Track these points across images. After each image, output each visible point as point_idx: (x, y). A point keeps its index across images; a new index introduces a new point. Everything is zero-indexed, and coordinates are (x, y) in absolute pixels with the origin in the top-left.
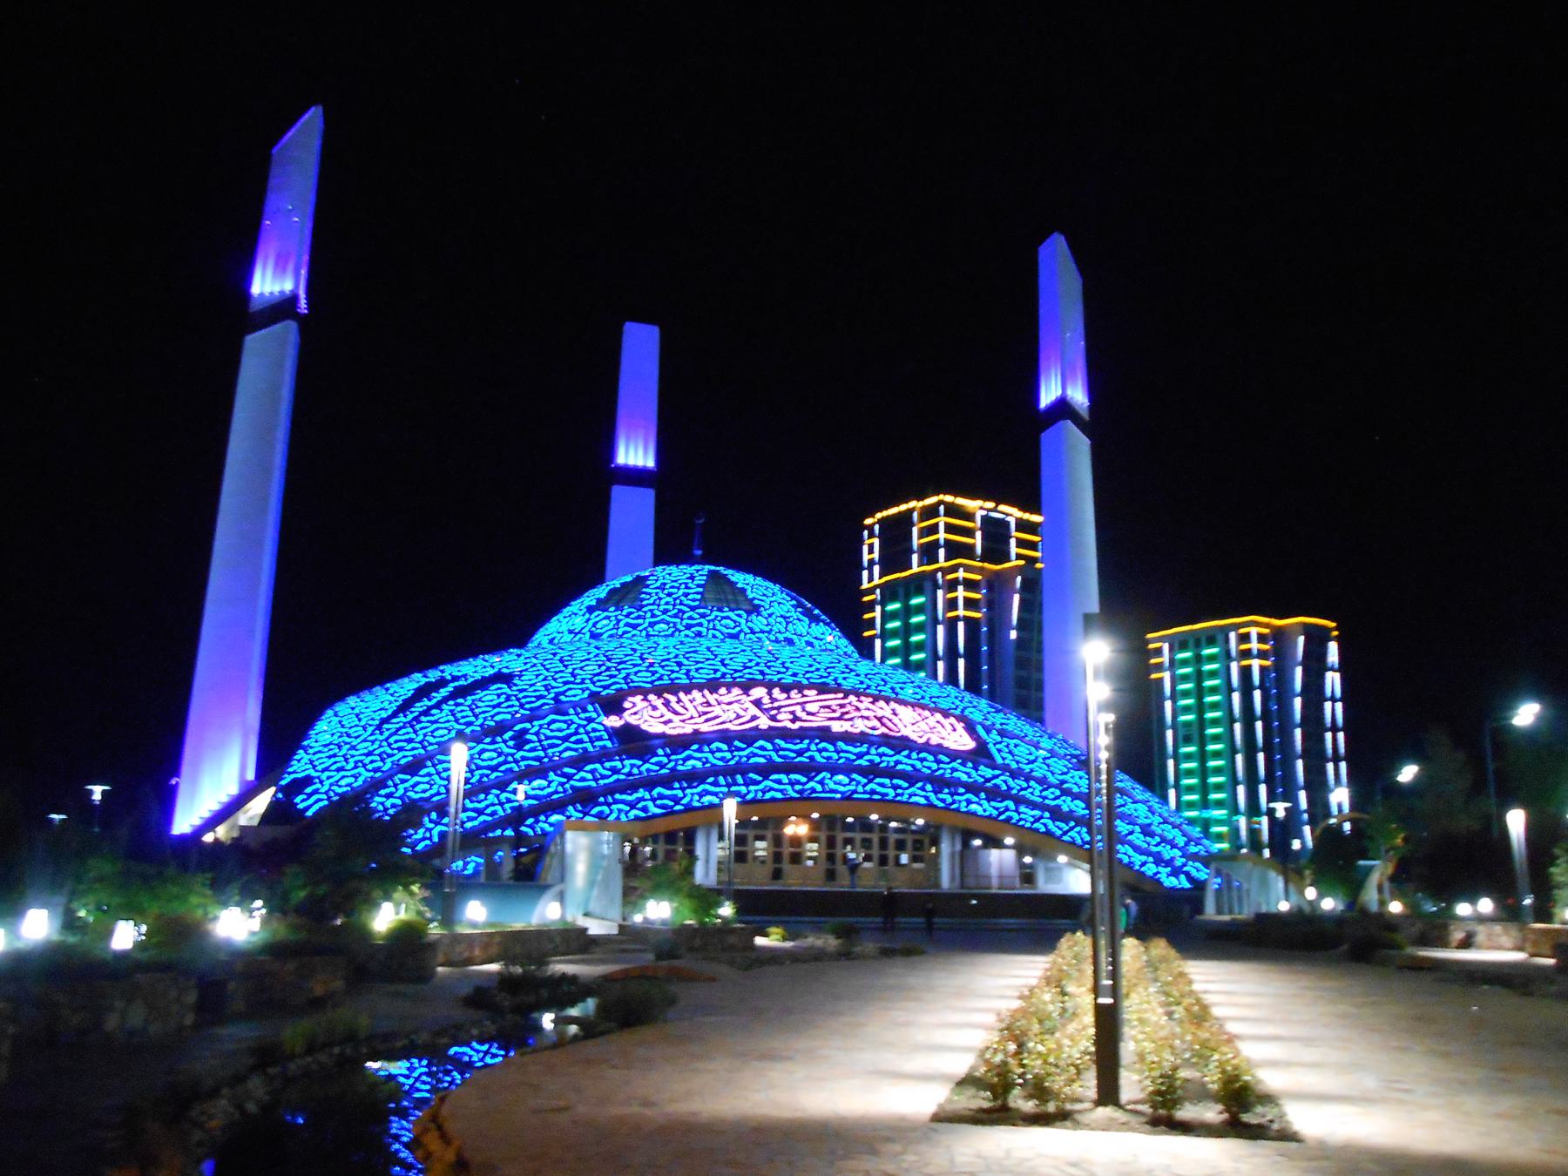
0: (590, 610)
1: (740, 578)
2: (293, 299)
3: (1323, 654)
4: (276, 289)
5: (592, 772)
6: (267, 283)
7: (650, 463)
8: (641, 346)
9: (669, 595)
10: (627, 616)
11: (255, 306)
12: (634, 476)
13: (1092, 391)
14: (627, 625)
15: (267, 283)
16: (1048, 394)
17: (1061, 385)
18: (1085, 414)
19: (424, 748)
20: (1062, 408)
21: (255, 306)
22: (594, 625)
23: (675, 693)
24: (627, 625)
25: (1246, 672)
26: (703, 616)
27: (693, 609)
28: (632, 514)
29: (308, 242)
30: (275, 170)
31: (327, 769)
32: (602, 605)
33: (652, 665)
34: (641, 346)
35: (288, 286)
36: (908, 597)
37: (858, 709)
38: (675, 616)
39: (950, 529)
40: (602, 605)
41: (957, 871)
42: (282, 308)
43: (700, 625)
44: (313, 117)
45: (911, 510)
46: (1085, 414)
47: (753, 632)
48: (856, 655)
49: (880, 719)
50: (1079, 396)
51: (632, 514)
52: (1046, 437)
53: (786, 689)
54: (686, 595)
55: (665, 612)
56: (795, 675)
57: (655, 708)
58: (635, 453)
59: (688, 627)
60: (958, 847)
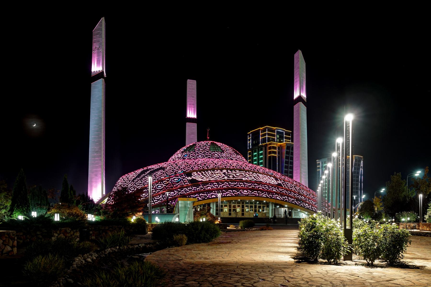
0: (182, 152)
1: (219, 144)
2: (103, 72)
5: (185, 190)
8: (192, 86)
9: (202, 148)
10: (192, 153)
11: (93, 75)
12: (191, 120)
14: (192, 156)
21: (93, 75)
24: (192, 156)
26: (210, 153)
27: (207, 151)
28: (191, 131)
34: (192, 86)
36: (259, 151)
38: (203, 153)
39: (269, 134)
42: (100, 75)
43: (210, 155)
49: (254, 177)
50: (304, 95)
51: (191, 131)
53: (231, 170)
54: (206, 148)
59: (206, 156)
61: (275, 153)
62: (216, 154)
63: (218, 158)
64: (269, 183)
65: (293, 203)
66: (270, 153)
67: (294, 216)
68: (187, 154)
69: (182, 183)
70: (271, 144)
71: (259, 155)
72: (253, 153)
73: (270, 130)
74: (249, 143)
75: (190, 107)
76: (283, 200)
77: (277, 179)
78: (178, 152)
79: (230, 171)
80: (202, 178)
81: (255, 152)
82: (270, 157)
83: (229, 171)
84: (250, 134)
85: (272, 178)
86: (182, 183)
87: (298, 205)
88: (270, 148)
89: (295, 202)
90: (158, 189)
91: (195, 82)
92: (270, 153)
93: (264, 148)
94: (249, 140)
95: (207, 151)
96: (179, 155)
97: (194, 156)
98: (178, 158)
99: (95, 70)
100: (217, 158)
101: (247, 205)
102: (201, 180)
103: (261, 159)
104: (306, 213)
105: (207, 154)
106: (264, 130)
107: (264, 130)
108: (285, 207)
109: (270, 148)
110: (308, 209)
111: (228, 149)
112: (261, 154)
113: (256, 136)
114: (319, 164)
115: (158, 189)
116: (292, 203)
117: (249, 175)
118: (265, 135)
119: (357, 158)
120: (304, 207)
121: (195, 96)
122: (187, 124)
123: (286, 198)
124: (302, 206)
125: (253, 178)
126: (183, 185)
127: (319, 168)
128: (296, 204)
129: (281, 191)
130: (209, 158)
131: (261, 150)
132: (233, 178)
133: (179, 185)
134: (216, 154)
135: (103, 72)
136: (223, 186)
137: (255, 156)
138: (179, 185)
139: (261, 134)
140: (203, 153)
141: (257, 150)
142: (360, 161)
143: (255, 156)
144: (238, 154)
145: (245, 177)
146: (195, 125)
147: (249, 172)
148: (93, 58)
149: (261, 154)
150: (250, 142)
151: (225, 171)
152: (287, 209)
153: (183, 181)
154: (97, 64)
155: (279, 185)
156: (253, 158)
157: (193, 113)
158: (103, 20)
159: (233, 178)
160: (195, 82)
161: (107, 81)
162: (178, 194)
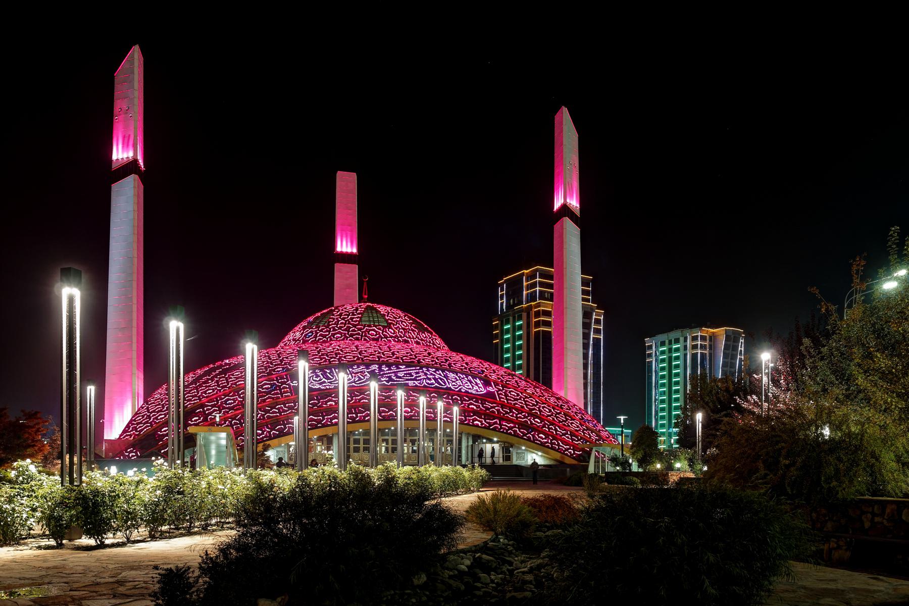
0: (304, 328)
1: (382, 309)
2: (135, 161)
3: (735, 348)
4: (125, 156)
5: (278, 409)
6: (120, 154)
7: (355, 251)
8: (346, 184)
9: (343, 319)
10: (321, 331)
11: (114, 166)
12: (346, 258)
13: (582, 201)
14: (321, 335)
15: (120, 154)
16: (558, 204)
17: (567, 197)
18: (578, 213)
19: (200, 399)
20: (565, 210)
21: (114, 166)
22: (305, 336)
23: (330, 369)
24: (321, 335)
25: (694, 356)
26: (359, 329)
27: (355, 326)
28: (346, 280)
29: (141, 129)
30: (118, 87)
31: (154, 411)
32: (310, 325)
33: (323, 355)
34: (346, 184)
35: (131, 154)
36: (514, 322)
37: (426, 374)
38: (345, 330)
39: (542, 284)
40: (310, 325)
41: (470, 455)
42: (130, 167)
43: (358, 334)
44: (135, 56)
45: (523, 274)
46: (578, 213)
47: (386, 337)
48: (446, 348)
49: (435, 379)
50: (574, 203)
51: (346, 280)
52: (557, 227)
53: (389, 366)
54: (352, 319)
55: (340, 328)
56: (397, 358)
57: (317, 376)
58: (345, 246)
59: (352, 335)
60: (470, 443)
61: (548, 324)
62: (374, 330)
63: (376, 340)
64: (467, 392)
65: (510, 434)
66: (538, 324)
67: (515, 461)
68: (312, 332)
69: (277, 394)
70: (538, 305)
71: (515, 329)
72: (502, 326)
73: (544, 275)
74: (502, 304)
75: (342, 230)
76: (488, 428)
77: (487, 383)
78: (297, 328)
79: (387, 366)
80: (320, 384)
81: (507, 323)
82: (537, 333)
83: (384, 368)
84: (502, 284)
85: (478, 381)
86: (277, 394)
87: (522, 438)
88: (538, 314)
89: (515, 431)
90: (225, 408)
91: (353, 177)
92: (538, 324)
93: (524, 315)
94: (502, 296)
95: (355, 326)
96: (298, 333)
97: (324, 336)
98: (294, 340)
99: (120, 157)
100: (373, 339)
101: (386, 437)
102: (318, 386)
103: (520, 338)
104: (540, 454)
105: (354, 331)
106: (532, 276)
107: (532, 276)
108: (494, 442)
109: (538, 314)
110: (543, 444)
111: (401, 319)
112: (520, 328)
113: (515, 289)
114: (650, 347)
115: (225, 408)
116: (507, 433)
117: (426, 374)
118: (533, 285)
119: (730, 334)
120: (533, 442)
121: (577, 165)
122: (337, 266)
123: (496, 423)
124: (529, 438)
125: (433, 381)
126: (278, 398)
127: (650, 355)
128: (516, 435)
129: (487, 409)
130: (357, 339)
131: (520, 318)
132: (388, 381)
133: (269, 398)
134: (374, 330)
135: (135, 161)
136: (360, 400)
137: (508, 331)
138: (269, 398)
139: (525, 284)
140: (345, 330)
141: (511, 318)
142: (736, 340)
143: (508, 331)
144: (424, 330)
145: (415, 379)
146: (356, 267)
147: (427, 368)
148: (115, 132)
149: (520, 328)
150: (502, 303)
151: (375, 367)
152: (496, 446)
153: (280, 390)
154: (123, 147)
155: (490, 395)
156: (502, 335)
157: (349, 244)
158: (135, 56)
159: (388, 381)
160: (353, 177)
161: (146, 178)
162: (264, 418)
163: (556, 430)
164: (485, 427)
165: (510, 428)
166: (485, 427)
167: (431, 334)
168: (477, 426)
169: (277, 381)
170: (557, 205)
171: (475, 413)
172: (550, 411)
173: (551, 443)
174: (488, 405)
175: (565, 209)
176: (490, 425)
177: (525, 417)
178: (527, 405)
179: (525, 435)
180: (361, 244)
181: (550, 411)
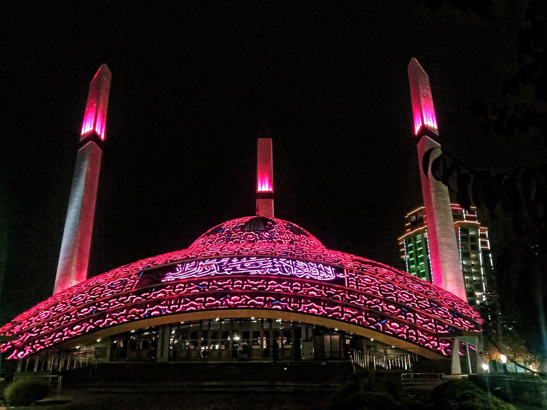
12: (265, 195)
28: (266, 210)
34: (265, 147)
43: (238, 238)
50: (431, 123)
51: (266, 210)
58: (264, 187)
62: (252, 234)
65: (354, 323)
77: (339, 270)
105: (235, 236)
120: (383, 332)
123: (337, 310)
129: (330, 295)
155: (339, 281)
163: (415, 318)
164: (322, 316)
165: (354, 316)
166: (323, 316)
167: (307, 236)
168: (313, 314)
169: (325, 290)
170: (417, 128)
171: (314, 299)
172: (411, 297)
173: (407, 334)
174: (332, 291)
175: (425, 130)
176: (329, 312)
177: (376, 303)
178: (381, 291)
179: (372, 323)
180: (276, 184)
181: (411, 297)
